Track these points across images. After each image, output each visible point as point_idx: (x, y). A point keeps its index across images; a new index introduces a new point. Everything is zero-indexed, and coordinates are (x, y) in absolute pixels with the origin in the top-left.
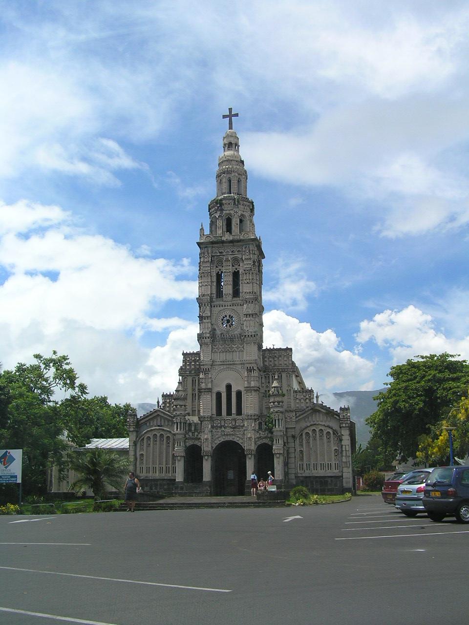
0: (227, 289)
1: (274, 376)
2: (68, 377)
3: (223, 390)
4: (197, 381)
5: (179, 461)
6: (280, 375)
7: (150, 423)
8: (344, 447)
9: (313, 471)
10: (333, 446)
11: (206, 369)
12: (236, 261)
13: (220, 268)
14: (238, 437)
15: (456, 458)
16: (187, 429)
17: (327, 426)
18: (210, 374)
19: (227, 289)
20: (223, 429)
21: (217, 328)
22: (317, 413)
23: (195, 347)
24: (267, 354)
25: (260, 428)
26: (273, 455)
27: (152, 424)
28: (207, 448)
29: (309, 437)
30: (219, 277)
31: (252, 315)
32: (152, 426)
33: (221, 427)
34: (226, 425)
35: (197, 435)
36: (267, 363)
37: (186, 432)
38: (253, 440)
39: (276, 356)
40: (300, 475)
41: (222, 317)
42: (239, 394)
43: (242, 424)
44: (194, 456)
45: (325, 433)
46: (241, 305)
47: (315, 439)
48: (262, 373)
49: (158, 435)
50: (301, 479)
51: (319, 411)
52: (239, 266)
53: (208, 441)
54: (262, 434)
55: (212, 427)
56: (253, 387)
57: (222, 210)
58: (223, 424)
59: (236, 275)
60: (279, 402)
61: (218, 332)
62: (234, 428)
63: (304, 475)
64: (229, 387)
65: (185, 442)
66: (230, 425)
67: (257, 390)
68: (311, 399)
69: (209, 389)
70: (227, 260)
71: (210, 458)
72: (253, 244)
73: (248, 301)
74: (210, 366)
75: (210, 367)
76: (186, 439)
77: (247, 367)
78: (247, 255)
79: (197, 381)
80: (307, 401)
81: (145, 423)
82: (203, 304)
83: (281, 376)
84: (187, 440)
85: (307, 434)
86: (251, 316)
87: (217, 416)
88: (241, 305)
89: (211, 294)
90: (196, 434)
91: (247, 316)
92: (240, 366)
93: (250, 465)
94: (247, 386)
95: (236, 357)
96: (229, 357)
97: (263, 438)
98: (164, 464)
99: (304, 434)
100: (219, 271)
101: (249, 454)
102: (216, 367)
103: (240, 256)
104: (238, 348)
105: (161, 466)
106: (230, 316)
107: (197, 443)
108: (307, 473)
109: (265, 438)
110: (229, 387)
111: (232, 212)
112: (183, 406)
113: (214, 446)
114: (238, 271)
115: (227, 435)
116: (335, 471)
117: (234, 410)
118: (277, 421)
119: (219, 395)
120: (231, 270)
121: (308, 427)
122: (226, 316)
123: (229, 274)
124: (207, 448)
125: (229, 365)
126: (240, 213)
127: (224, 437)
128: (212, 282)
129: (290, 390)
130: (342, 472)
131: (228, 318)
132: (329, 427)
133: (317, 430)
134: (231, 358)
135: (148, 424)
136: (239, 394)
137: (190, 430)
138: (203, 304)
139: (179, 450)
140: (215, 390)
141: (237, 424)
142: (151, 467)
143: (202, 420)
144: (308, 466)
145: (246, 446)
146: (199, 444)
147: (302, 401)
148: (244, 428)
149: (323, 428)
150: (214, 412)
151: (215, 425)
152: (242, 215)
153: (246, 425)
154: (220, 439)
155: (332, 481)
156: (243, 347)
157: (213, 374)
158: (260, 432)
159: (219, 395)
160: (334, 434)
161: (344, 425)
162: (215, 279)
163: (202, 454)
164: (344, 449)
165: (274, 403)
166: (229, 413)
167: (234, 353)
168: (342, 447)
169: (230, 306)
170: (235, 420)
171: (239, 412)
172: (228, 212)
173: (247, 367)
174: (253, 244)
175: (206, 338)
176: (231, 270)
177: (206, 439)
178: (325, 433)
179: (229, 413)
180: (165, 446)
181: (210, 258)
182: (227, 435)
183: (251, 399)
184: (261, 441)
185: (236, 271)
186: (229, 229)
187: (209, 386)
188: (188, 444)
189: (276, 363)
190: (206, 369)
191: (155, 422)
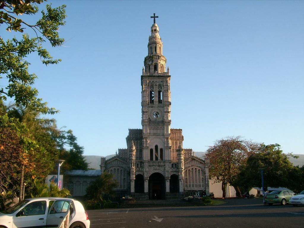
1: (176, 142)
2: (72, 138)
3: (154, 148)
4: (139, 143)
8: (206, 177)
9: (192, 188)
10: (201, 176)
13: (152, 89)
14: (161, 171)
15: (192, 197)
17: (199, 167)
20: (154, 167)
22: (194, 160)
23: (139, 126)
28: (147, 176)
29: (190, 172)
33: (153, 165)
34: (156, 165)
40: (186, 190)
42: (161, 150)
45: (197, 170)
46: (162, 107)
49: (116, 169)
50: (187, 191)
51: (195, 159)
52: (161, 88)
53: (148, 172)
54: (175, 170)
57: (152, 61)
63: (187, 190)
64: (156, 147)
68: (191, 154)
69: (148, 147)
70: (156, 85)
71: (148, 181)
79: (139, 143)
80: (190, 154)
81: (110, 163)
85: (189, 170)
87: (151, 160)
88: (162, 107)
90: (141, 169)
92: (162, 137)
93: (168, 184)
97: (174, 172)
99: (188, 171)
104: (161, 128)
106: (157, 112)
108: (189, 189)
110: (156, 147)
116: (202, 188)
117: (159, 158)
121: (189, 167)
124: (147, 176)
127: (155, 171)
130: (206, 188)
132: (199, 167)
133: (194, 169)
136: (161, 150)
140: (150, 148)
141: (161, 165)
142: (122, 184)
144: (190, 185)
145: (166, 176)
146: (142, 174)
147: (187, 154)
158: (172, 169)
159: (151, 150)
160: (202, 170)
161: (207, 166)
164: (206, 178)
168: (205, 177)
176: (158, 90)
178: (197, 170)
180: (119, 175)
191: (115, 162)
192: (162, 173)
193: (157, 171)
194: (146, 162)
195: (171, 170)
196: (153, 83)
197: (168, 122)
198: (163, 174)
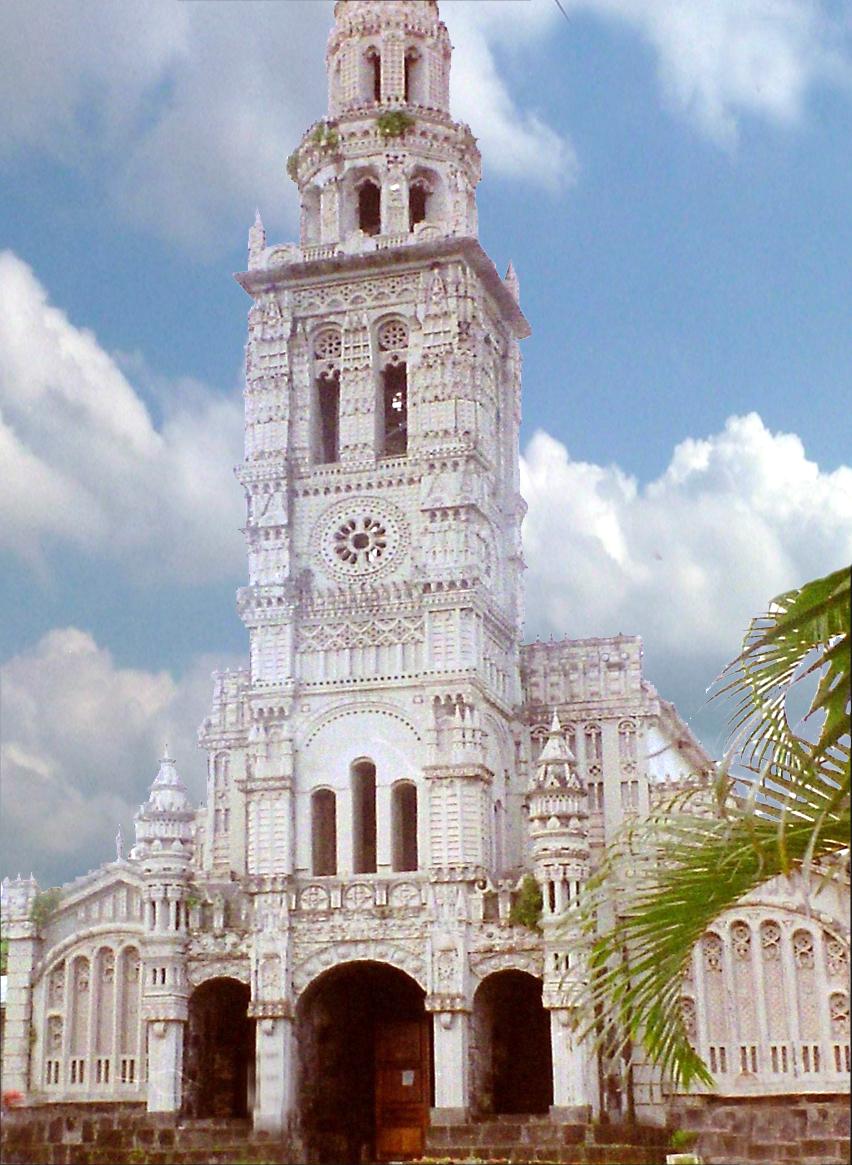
0: (358, 426)
5: (161, 1036)
6: (593, 732)
7: (88, 910)
11: (271, 710)
12: (391, 328)
16: (195, 923)
18: (285, 728)
19: (358, 426)
21: (315, 569)
24: (539, 662)
25: (490, 916)
26: (544, 1016)
27: (95, 915)
28: (272, 990)
30: (328, 392)
31: (457, 513)
32: (99, 921)
35: (235, 945)
36: (537, 693)
37: (188, 934)
38: (462, 957)
39: (575, 668)
41: (335, 529)
42: (406, 797)
43: (415, 903)
44: (219, 1022)
45: (787, 934)
47: (745, 955)
48: (517, 726)
50: (689, 1102)
53: (275, 970)
54: (501, 938)
55: (295, 913)
56: (458, 766)
58: (336, 902)
59: (394, 379)
60: (564, 818)
61: (321, 582)
62: (384, 913)
64: (365, 774)
65: (186, 971)
66: (369, 904)
67: (481, 778)
71: (460, 1020)
72: (459, 262)
73: (437, 465)
74: (290, 699)
75: (286, 703)
76: (191, 959)
77: (437, 698)
78: (436, 303)
82: (261, 486)
83: (599, 735)
84: (193, 965)
86: (451, 517)
89: (291, 449)
91: (433, 515)
94: (434, 764)
95: (392, 662)
96: (366, 664)
98: (138, 1051)
100: (325, 369)
101: (442, 1012)
102: (315, 703)
103: (406, 310)
105: (128, 1058)
107: (231, 971)
109: (511, 951)
110: (365, 774)
111: (380, 162)
112: (177, 844)
113: (304, 982)
114: (403, 365)
115: (356, 942)
118: (558, 886)
119: (324, 801)
120: (370, 362)
122: (353, 525)
123: (364, 374)
125: (363, 692)
126: (410, 163)
128: (293, 406)
129: (635, 782)
131: (360, 529)
133: (755, 925)
134: (373, 668)
135: (82, 915)
137: (206, 925)
138: (261, 486)
139: (162, 999)
140: (310, 783)
143: (254, 889)
145: (427, 983)
148: (424, 917)
149: (778, 916)
150: (305, 859)
151: (305, 906)
152: (423, 172)
153: (430, 905)
154: (324, 957)
155: (824, 1114)
156: (421, 628)
157: (300, 724)
160: (827, 936)
162: (307, 398)
163: (250, 1015)
165: (544, 819)
166: (366, 861)
167: (384, 651)
169: (380, 485)
170: (389, 887)
171: (407, 858)
172: (362, 162)
173: (437, 698)
174: (459, 262)
175: (270, 603)
177: (272, 957)
178: (787, 934)
179: (366, 861)
181: (288, 325)
182: (356, 942)
183: (452, 809)
184: (493, 962)
185: (396, 364)
186: (369, 215)
187: (284, 768)
188: (199, 978)
189: (578, 689)
190: (271, 710)
192: (408, 968)
193: (372, 954)
194: (268, 888)
195: (483, 942)
196: (332, 318)
197: (440, 585)
198: (417, 971)
